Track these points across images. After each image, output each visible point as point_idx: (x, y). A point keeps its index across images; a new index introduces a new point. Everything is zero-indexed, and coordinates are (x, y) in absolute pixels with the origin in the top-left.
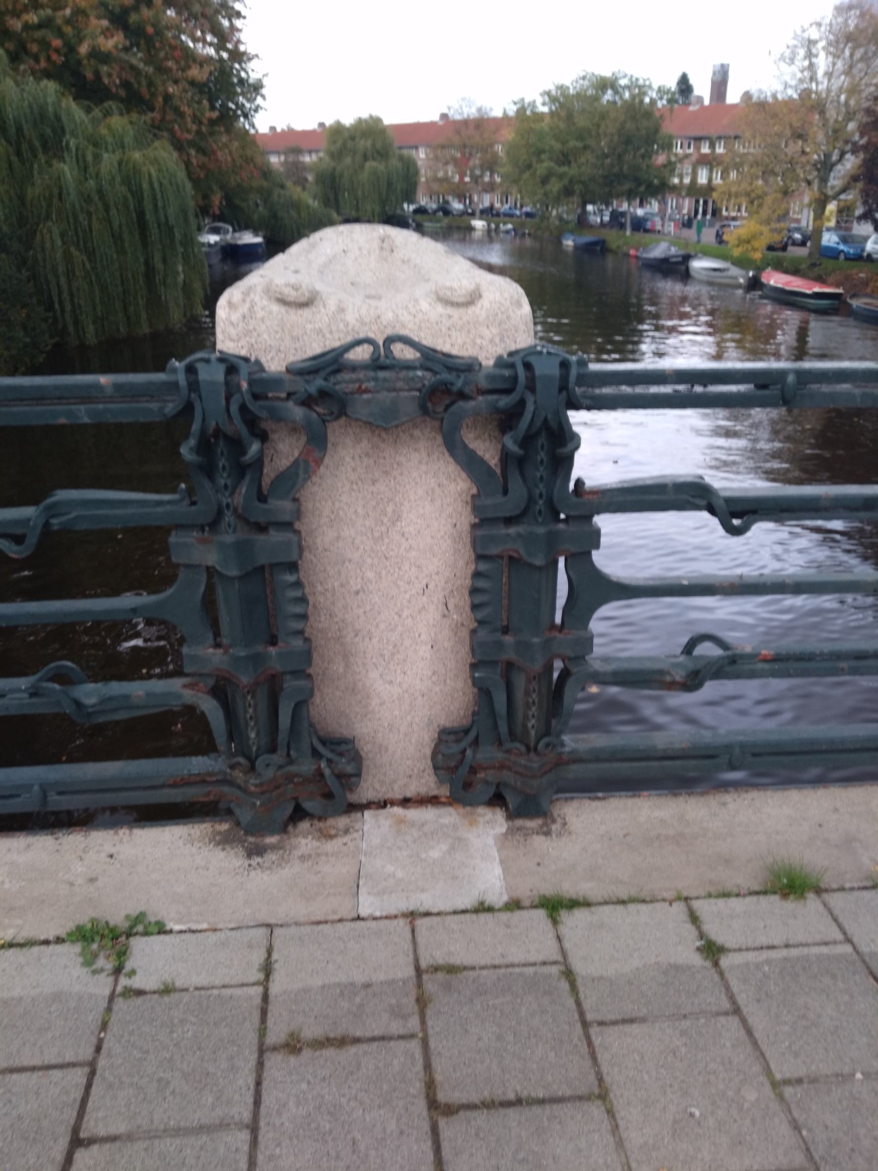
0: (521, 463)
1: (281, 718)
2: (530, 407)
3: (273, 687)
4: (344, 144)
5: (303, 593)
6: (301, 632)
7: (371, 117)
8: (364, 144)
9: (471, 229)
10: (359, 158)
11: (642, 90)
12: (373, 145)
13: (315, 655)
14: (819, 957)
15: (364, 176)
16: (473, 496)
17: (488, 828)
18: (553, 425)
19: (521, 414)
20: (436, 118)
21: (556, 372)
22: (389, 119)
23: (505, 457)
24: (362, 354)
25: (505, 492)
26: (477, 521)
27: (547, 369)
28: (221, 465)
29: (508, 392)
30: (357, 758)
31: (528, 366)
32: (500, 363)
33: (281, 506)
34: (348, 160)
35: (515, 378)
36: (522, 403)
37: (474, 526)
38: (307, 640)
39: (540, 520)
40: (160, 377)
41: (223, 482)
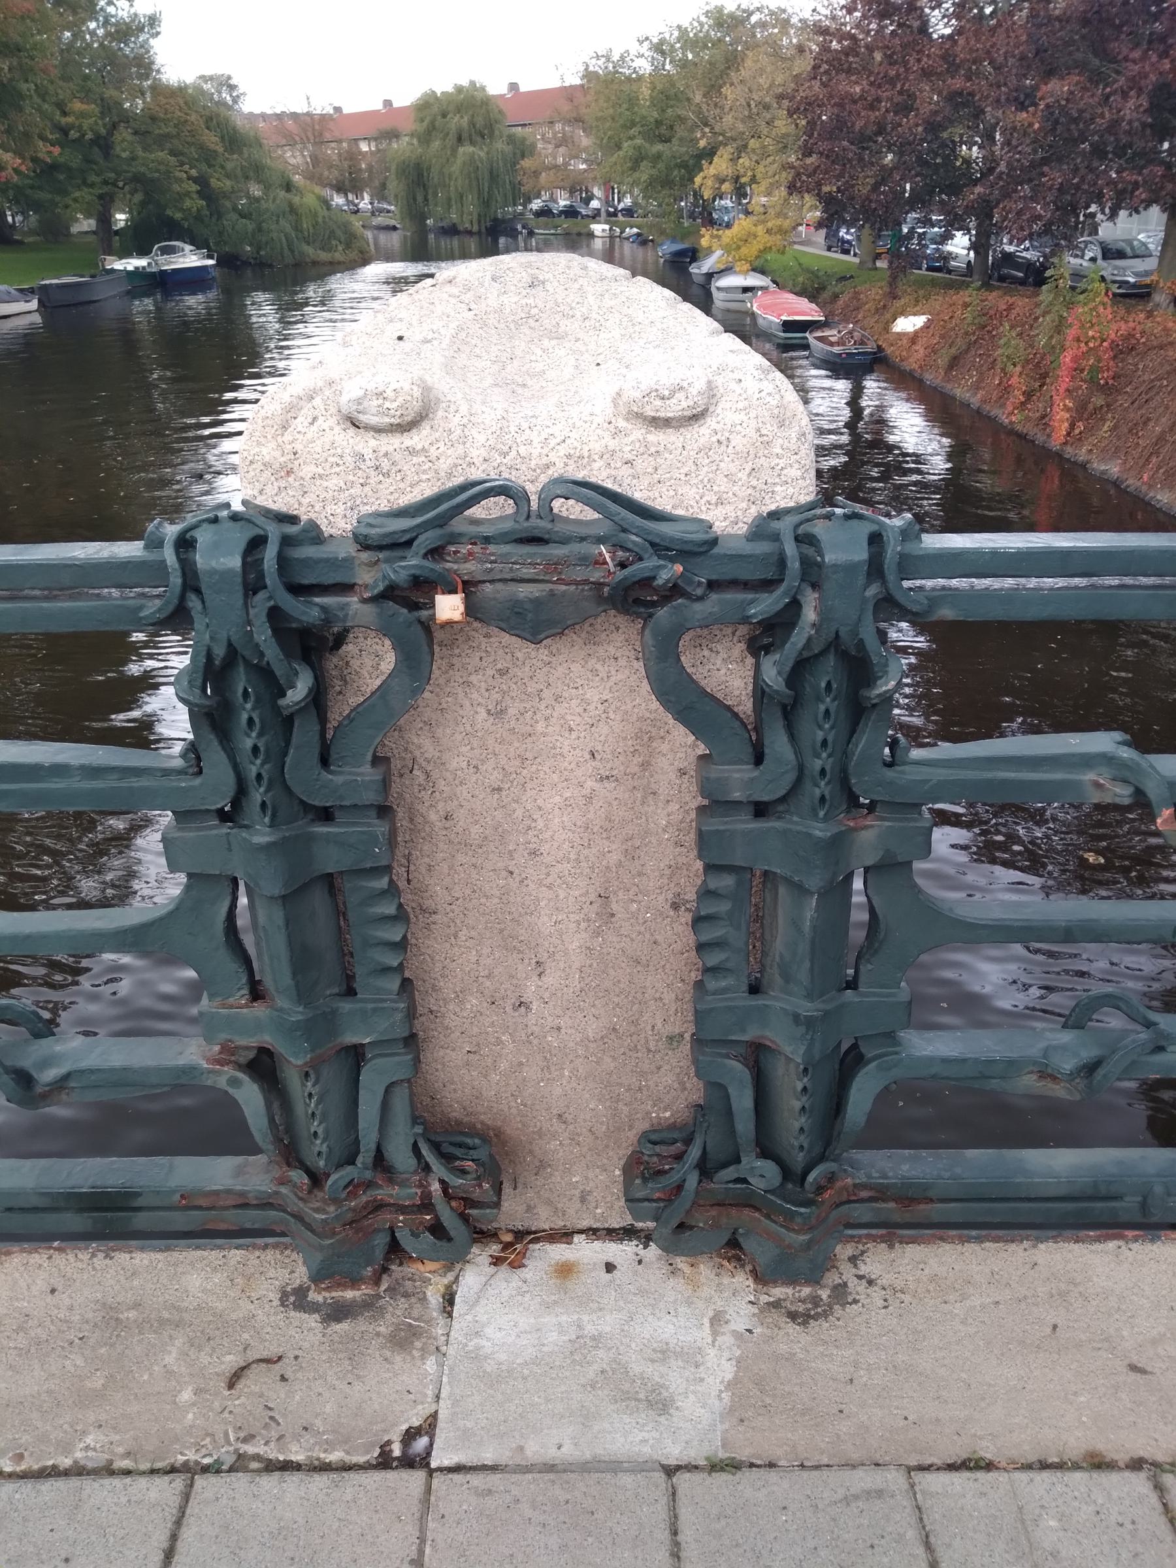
0: (789, 712)
1: (362, 1108)
2: (810, 614)
4: (433, 123)
7: (473, 83)
8: (459, 121)
9: (591, 235)
10: (451, 140)
12: (472, 124)
15: (455, 168)
20: (379, 106)
21: (861, 554)
22: (496, 87)
23: (760, 693)
24: (491, 511)
25: (759, 759)
26: (706, 802)
27: (843, 547)
28: (245, 716)
29: (767, 585)
31: (805, 540)
33: (355, 776)
34: (436, 144)
35: (782, 562)
36: (795, 605)
37: (701, 810)
39: (822, 814)
40: (128, 550)
41: (249, 743)
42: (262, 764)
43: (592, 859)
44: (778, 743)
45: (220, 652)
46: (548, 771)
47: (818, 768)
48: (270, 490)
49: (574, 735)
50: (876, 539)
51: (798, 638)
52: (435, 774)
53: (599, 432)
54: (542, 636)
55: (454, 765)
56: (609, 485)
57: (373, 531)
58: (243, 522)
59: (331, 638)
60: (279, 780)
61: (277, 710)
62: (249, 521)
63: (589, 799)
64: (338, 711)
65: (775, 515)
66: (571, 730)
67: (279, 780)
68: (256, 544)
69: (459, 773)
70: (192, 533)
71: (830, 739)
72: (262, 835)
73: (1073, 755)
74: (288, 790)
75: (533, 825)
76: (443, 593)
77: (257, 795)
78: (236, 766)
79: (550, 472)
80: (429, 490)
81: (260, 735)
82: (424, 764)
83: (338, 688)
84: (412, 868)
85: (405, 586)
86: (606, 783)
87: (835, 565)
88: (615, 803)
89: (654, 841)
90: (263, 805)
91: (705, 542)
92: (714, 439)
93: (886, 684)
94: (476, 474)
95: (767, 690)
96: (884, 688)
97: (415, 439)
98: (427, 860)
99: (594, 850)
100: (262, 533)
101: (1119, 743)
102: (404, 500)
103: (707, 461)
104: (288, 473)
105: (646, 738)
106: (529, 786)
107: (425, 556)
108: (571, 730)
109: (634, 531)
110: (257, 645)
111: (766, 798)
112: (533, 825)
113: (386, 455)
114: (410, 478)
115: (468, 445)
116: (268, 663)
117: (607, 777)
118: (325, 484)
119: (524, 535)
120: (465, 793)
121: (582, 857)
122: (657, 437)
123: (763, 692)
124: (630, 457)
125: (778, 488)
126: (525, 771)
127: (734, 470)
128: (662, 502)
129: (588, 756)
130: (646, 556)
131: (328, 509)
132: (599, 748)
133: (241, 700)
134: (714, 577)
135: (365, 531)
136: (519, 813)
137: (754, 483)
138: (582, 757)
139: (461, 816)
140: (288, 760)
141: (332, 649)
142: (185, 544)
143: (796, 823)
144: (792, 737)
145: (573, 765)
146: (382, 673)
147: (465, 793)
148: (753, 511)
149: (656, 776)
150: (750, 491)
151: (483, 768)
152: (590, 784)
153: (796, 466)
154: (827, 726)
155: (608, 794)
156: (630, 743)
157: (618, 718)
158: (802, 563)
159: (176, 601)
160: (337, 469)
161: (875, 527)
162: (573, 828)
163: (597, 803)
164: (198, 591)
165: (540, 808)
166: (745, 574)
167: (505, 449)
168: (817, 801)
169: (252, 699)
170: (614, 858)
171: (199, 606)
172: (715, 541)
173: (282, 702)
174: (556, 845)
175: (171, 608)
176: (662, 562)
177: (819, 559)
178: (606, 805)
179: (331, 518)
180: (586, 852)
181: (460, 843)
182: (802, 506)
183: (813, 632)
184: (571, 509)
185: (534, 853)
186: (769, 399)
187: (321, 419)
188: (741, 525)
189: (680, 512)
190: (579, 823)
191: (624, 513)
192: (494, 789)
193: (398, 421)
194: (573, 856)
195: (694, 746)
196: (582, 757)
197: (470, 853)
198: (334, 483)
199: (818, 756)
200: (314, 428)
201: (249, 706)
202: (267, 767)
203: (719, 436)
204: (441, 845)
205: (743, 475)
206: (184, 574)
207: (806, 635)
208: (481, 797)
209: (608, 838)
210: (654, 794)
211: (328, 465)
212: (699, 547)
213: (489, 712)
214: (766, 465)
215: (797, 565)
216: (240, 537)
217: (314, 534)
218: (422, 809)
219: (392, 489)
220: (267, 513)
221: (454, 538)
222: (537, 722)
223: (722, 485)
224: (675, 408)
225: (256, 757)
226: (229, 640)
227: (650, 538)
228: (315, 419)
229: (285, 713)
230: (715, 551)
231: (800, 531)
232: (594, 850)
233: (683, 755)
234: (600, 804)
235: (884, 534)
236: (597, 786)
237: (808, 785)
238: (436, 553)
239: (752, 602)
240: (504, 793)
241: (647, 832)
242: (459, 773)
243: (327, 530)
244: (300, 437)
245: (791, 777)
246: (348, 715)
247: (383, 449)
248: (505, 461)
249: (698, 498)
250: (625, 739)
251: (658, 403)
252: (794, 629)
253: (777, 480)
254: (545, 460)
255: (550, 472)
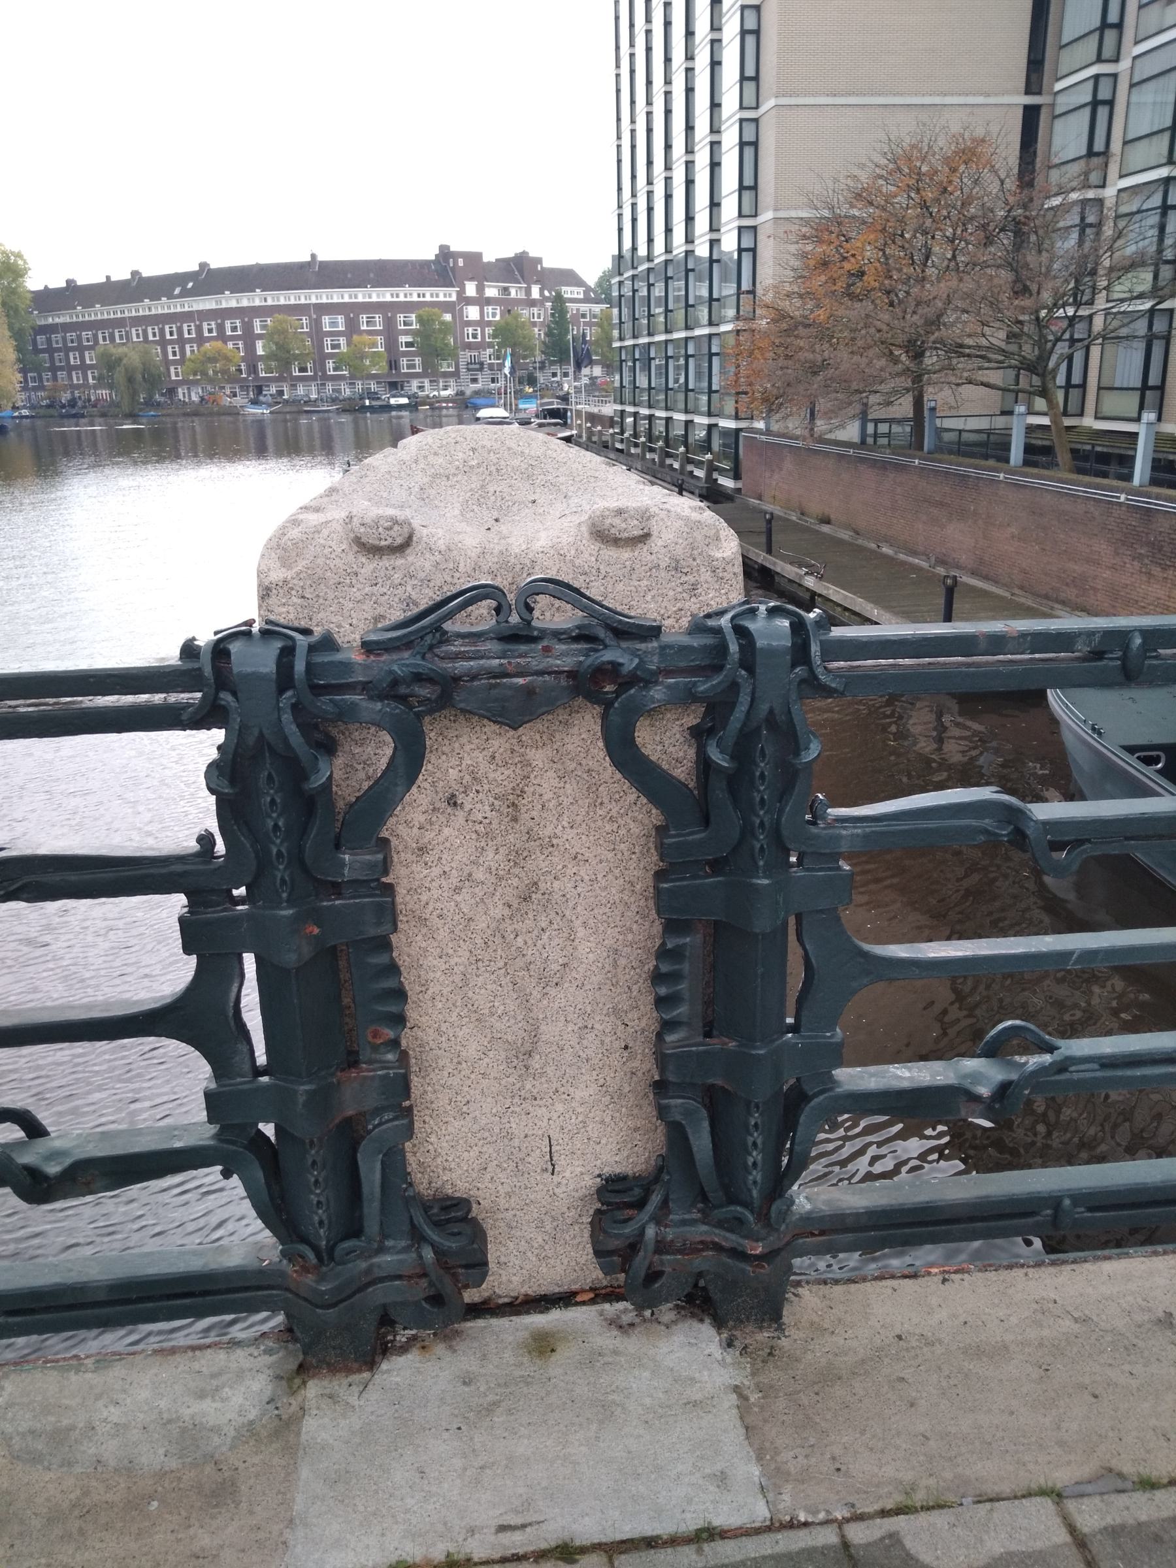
3: (349, 1136)
5: (392, 959)
6: (395, 1043)
11: (328, 643)
13: (415, 1081)
14: (698, 1054)
16: (658, 829)
17: (691, 1356)
18: (781, 718)
19: (732, 705)
24: (481, 616)
25: (706, 821)
30: (478, 1234)
32: (698, 627)
35: (722, 648)
36: (734, 687)
37: (660, 876)
38: (404, 1056)
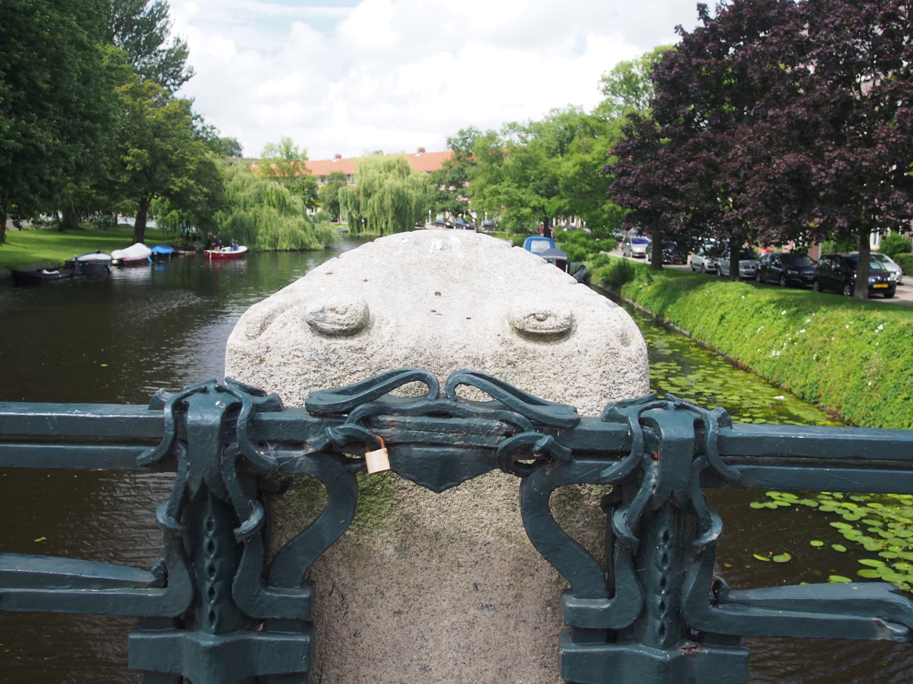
28: (207, 540)
42: (216, 581)
43: (472, 675)
44: (626, 581)
45: (195, 488)
46: (439, 598)
47: (659, 602)
48: (247, 373)
49: (462, 570)
50: (699, 424)
51: (642, 496)
52: (349, 597)
53: (491, 341)
54: (443, 487)
55: (363, 591)
56: (497, 377)
57: (321, 403)
58: (225, 393)
59: (279, 484)
60: (226, 594)
61: (232, 536)
62: (230, 392)
63: (471, 624)
64: (281, 540)
65: (622, 404)
66: (459, 566)
67: (226, 594)
68: (233, 409)
69: (368, 597)
70: (188, 400)
71: (668, 579)
72: (207, 639)
73: (857, 600)
74: (232, 602)
75: (425, 644)
76: (371, 451)
77: (209, 606)
78: (194, 581)
79: (454, 368)
80: (361, 378)
81: (216, 557)
82: (341, 589)
83: (279, 524)
84: (324, 677)
85: (342, 444)
86: (486, 611)
87: (669, 442)
88: (492, 628)
89: (523, 661)
90: (212, 615)
91: (571, 421)
92: (576, 349)
93: (711, 534)
94: (397, 367)
95: (618, 536)
96: (709, 539)
97: (354, 342)
98: (337, 671)
99: (474, 668)
100: (238, 401)
101: (891, 592)
102: (345, 384)
103: (570, 365)
104: (262, 361)
105: (519, 574)
106: (423, 610)
107: (358, 423)
108: (459, 566)
109: (518, 409)
110: (224, 485)
111: (617, 627)
112: (425, 644)
113: (333, 352)
114: (351, 366)
115: (394, 347)
116: (230, 499)
117: (487, 606)
118: (287, 370)
119: (430, 411)
120: (372, 614)
121: (463, 674)
122: (531, 346)
123: (614, 538)
124: (513, 359)
125: (622, 387)
126: (421, 599)
127: (590, 372)
128: (537, 392)
129: (472, 588)
130: (526, 429)
131: (287, 387)
132: (482, 582)
133: (205, 528)
134: (578, 447)
135: (313, 402)
136: (414, 633)
137: (605, 382)
138: (467, 588)
139: (366, 634)
140: (236, 577)
141: (278, 493)
142: (180, 407)
143: (641, 649)
144: (638, 576)
145: (460, 595)
146: (315, 513)
147: (372, 614)
148: (605, 402)
149: (526, 607)
150: (602, 387)
151: (387, 594)
152: (472, 611)
153: (636, 371)
154: (665, 568)
155: (487, 620)
156: (506, 578)
157: (498, 557)
158: (645, 439)
159: (167, 448)
160: (297, 360)
161: (698, 416)
162: (457, 648)
163: (477, 628)
164: (185, 442)
165: (431, 630)
166: (601, 447)
167: (421, 350)
168: (657, 631)
169: (214, 527)
170: (490, 675)
171: (184, 452)
172: (577, 421)
173: (237, 531)
174: (442, 662)
175: (162, 454)
176: (540, 434)
177: (657, 437)
178: (485, 630)
179: (289, 394)
180: (467, 670)
181: (365, 657)
182: (641, 399)
183: (654, 492)
184: (471, 394)
185: (425, 669)
186: (614, 324)
187: (289, 325)
188: (595, 412)
189: (550, 400)
190: (462, 644)
191: (510, 396)
192: (395, 613)
193: (345, 328)
194: (456, 673)
195: (558, 582)
196: (467, 588)
197: (372, 666)
198: (292, 369)
199: (659, 593)
200: (284, 331)
201: (211, 533)
202: (218, 583)
203: (579, 348)
204: (349, 658)
205: (597, 376)
206: (176, 430)
207: (648, 494)
208: (384, 618)
209: (486, 658)
210: (524, 621)
211: (291, 356)
212: (566, 427)
213: (396, 548)
214: (613, 369)
215: (641, 440)
216: (221, 404)
217: (276, 403)
218: (337, 626)
219: (336, 376)
220: (244, 388)
221: (385, 410)
222: (433, 558)
223: (582, 381)
224: (549, 326)
225: (211, 575)
226: (203, 480)
227: (530, 415)
228: (285, 324)
229: (239, 540)
230: (579, 427)
231: (644, 415)
232: (474, 668)
233: (548, 590)
234: (480, 628)
235: (705, 421)
236: (478, 613)
237: (651, 617)
238: (366, 420)
239: (607, 466)
240: (403, 616)
241: (518, 655)
242: (368, 597)
243: (286, 404)
244: (273, 336)
245: (637, 609)
246: (286, 545)
247: (333, 347)
248: (421, 359)
249: (563, 391)
250: (502, 575)
251: (536, 322)
252: (638, 488)
253: (622, 381)
254: (451, 360)
255: (454, 368)
